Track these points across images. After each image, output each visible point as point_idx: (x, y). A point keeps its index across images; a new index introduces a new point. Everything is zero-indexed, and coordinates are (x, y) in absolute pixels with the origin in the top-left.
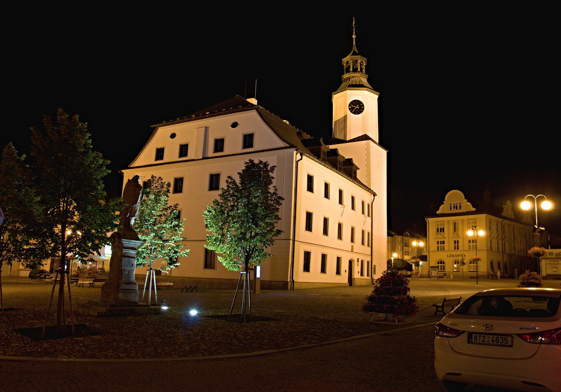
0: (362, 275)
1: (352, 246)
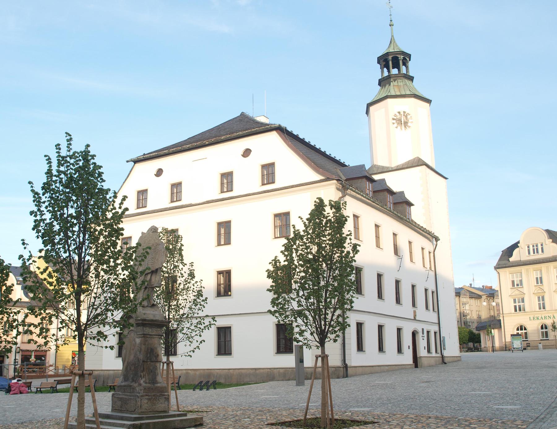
0: (429, 351)
1: (415, 312)
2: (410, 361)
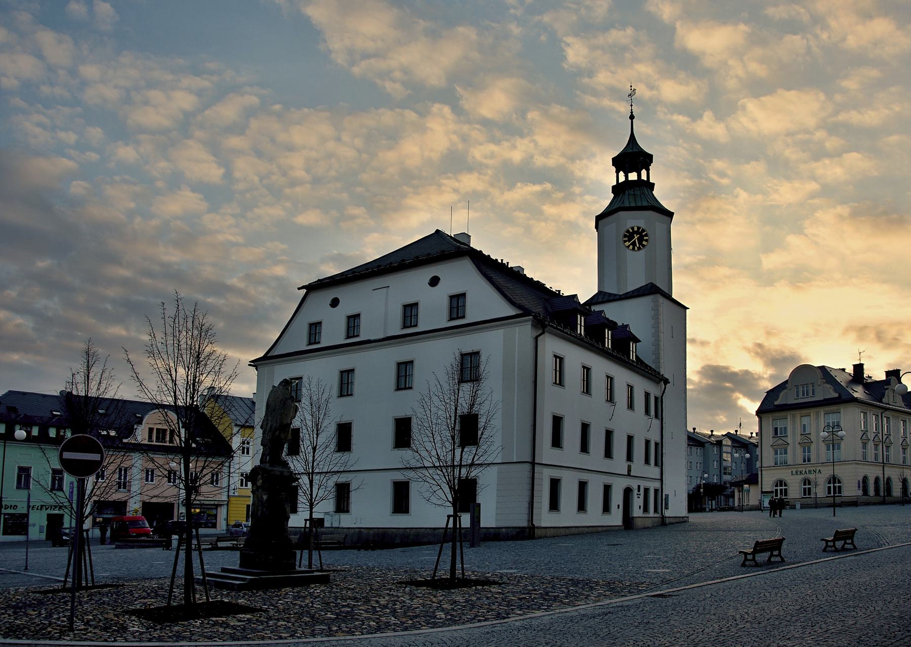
0: (646, 510)
2: (619, 522)
